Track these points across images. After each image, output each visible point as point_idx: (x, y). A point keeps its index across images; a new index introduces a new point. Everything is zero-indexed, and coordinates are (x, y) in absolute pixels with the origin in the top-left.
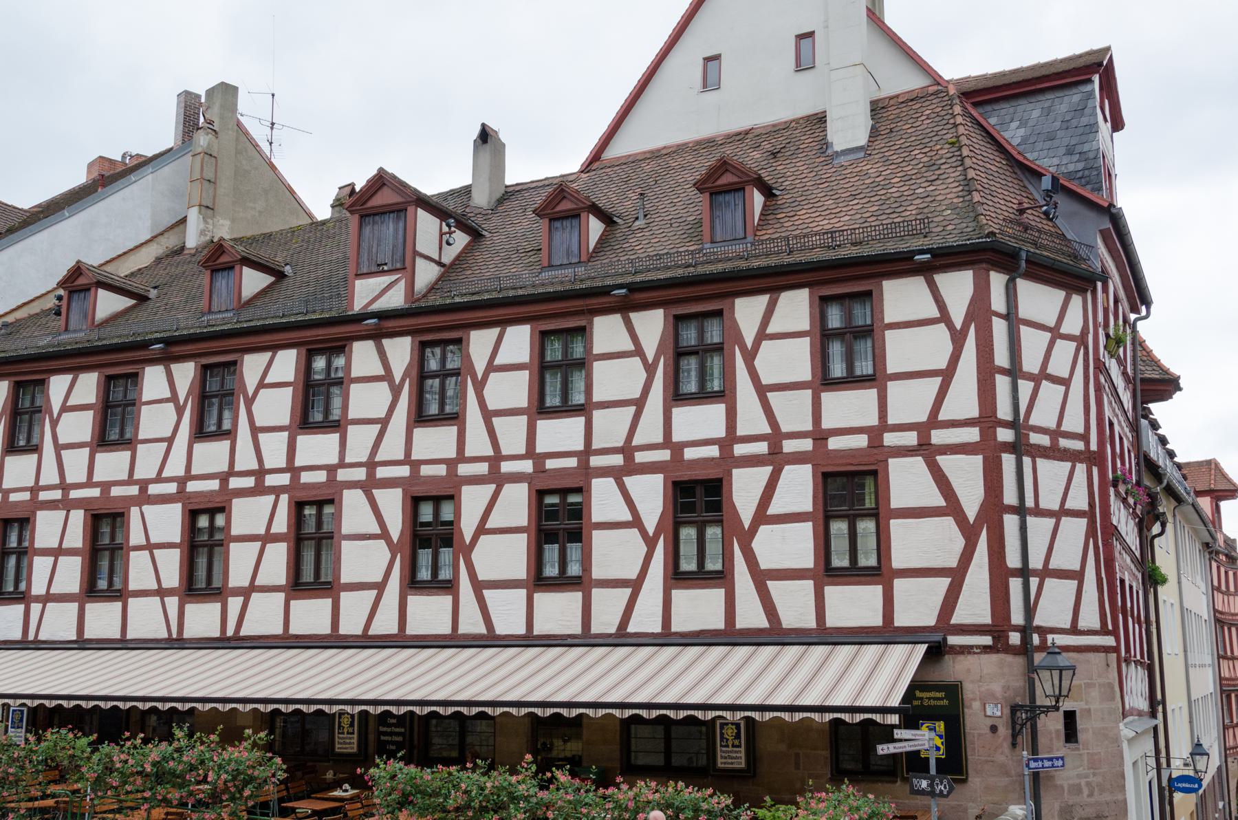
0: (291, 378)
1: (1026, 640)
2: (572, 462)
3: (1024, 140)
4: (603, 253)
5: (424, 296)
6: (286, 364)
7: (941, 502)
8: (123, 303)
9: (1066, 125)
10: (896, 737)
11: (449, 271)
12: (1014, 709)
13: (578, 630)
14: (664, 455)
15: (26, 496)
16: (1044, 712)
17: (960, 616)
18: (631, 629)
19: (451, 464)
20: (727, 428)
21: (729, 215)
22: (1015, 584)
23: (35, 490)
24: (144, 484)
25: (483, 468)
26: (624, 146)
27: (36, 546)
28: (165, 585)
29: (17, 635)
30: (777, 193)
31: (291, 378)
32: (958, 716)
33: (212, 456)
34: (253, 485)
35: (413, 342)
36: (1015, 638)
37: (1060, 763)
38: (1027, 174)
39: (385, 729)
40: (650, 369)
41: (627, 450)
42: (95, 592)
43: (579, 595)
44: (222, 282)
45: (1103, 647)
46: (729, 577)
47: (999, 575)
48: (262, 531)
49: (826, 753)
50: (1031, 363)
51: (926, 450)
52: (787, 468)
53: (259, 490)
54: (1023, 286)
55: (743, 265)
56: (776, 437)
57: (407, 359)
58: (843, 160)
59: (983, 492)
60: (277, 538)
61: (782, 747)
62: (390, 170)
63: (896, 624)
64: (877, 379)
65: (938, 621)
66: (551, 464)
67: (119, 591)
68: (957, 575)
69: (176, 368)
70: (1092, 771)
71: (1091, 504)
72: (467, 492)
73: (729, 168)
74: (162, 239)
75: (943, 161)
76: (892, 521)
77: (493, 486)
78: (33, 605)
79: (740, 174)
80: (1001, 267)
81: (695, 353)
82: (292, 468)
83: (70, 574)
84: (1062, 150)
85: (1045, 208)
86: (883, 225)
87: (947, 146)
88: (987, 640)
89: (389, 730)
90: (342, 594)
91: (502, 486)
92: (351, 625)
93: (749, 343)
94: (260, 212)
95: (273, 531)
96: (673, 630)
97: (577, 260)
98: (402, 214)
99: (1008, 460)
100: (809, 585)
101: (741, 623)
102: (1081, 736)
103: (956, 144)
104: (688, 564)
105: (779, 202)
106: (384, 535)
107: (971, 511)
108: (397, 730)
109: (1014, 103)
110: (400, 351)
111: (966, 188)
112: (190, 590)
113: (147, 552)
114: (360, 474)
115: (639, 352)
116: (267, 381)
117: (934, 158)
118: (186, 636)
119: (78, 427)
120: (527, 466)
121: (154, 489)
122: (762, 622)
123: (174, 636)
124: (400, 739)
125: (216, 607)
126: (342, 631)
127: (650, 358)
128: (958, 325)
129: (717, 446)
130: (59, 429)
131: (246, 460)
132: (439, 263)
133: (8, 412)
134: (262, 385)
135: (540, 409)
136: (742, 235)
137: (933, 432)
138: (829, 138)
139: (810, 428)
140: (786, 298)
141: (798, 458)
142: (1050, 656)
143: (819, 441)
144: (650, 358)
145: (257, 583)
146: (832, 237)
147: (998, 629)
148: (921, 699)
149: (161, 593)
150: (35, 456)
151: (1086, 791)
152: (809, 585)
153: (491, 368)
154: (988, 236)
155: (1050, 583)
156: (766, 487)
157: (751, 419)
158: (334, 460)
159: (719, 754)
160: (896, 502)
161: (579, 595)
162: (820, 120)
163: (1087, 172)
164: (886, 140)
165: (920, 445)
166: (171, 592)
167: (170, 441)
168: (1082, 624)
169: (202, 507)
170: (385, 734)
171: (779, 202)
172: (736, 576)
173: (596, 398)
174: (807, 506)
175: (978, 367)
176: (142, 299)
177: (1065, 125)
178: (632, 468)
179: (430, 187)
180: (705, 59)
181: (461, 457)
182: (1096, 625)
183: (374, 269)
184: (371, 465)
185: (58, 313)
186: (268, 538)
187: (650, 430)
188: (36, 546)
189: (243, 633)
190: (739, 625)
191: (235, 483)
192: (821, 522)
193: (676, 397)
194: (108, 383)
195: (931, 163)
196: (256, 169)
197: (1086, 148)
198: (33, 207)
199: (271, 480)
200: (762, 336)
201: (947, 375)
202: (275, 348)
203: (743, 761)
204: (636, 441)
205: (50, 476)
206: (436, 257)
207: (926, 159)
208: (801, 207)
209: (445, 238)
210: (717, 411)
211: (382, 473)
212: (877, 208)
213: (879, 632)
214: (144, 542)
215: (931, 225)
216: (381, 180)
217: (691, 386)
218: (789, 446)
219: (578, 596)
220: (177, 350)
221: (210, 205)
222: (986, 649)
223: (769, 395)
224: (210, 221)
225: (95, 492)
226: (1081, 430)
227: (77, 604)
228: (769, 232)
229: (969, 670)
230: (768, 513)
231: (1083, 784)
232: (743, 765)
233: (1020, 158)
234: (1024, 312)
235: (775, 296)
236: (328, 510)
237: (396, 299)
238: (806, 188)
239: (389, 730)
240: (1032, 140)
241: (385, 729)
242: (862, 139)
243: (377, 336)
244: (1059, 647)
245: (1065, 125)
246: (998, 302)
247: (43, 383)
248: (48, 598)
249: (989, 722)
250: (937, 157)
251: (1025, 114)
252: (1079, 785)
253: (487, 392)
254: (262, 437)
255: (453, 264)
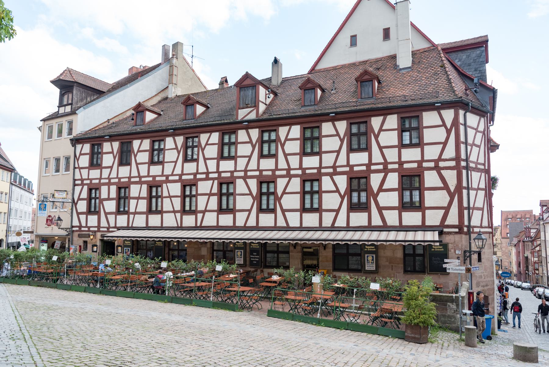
0: (217, 142)
1: (469, 230)
2: (315, 171)
3: (461, 65)
4: (322, 102)
5: (262, 115)
6: (215, 137)
7: (442, 185)
8: (154, 116)
9: (475, 61)
10: (445, 261)
11: (269, 106)
12: (465, 252)
13: (318, 225)
14: (347, 169)
15: (127, 180)
16: (475, 253)
17: (448, 222)
18: (336, 225)
19: (273, 171)
20: (369, 160)
21: (367, 89)
22: (466, 212)
23: (130, 178)
24: (167, 176)
25: (284, 173)
26: (326, 64)
27: (131, 196)
28: (176, 209)
29: (126, 225)
30: (381, 82)
31: (217, 142)
32: (447, 254)
33: (190, 167)
34: (205, 177)
35: (259, 130)
36: (465, 229)
37: (478, 269)
38: (465, 78)
39: (253, 256)
40: (342, 141)
41: (334, 167)
42: (151, 211)
43: (318, 214)
44: (189, 109)
45: (489, 232)
46: (369, 209)
47: (461, 209)
48: (209, 192)
49: (402, 265)
50: (470, 141)
51: (437, 168)
52: (389, 174)
53: (207, 179)
54: (468, 114)
55: (374, 106)
56: (386, 163)
57: (257, 136)
58: (403, 71)
59: (456, 182)
60: (214, 195)
61: (387, 263)
62: (249, 72)
63: (426, 225)
64: (420, 144)
65: (440, 224)
66: (308, 171)
67: (160, 211)
68: (447, 209)
69: (177, 138)
70: (485, 271)
71: (486, 187)
72: (279, 180)
73: (367, 73)
74: (160, 95)
75: (440, 72)
76: (425, 191)
77: (288, 179)
78: (130, 215)
79: (371, 76)
80: (463, 109)
81: (409, 131)
82: (218, 172)
83: (143, 206)
84: (474, 70)
85: (475, 89)
86: (417, 94)
87: (439, 67)
88: (457, 230)
89: (254, 257)
90: (237, 213)
91: (291, 178)
92: (240, 222)
93: (376, 132)
94: (190, 86)
95: (212, 192)
96: (350, 226)
97: (314, 104)
98: (254, 87)
99: (464, 172)
100: (397, 212)
101: (278, 225)
102: (482, 260)
103: (443, 66)
104: (264, 206)
105: (383, 85)
106: (251, 194)
107: (452, 189)
108: (257, 257)
109: (457, 53)
110: (255, 133)
111: (449, 82)
112: (119, 211)
113: (169, 199)
114: (242, 174)
115: (338, 134)
116: (209, 143)
117: (436, 71)
118: (164, 226)
119: (144, 157)
120: (299, 172)
121: (171, 178)
122: (381, 223)
123: (179, 226)
124: (258, 260)
125: (193, 217)
126: (237, 225)
127: (342, 137)
128: (449, 127)
129: (365, 166)
130: (137, 158)
131: (202, 169)
132: (266, 104)
133: (119, 152)
134: (207, 144)
135: (303, 153)
136: (372, 96)
137: (440, 163)
138: (398, 64)
139: (398, 161)
140: (294, 127)
141: (393, 171)
142: (479, 235)
143: (401, 165)
144: (342, 137)
145: (207, 209)
146: (405, 97)
147: (460, 227)
148: (367, 248)
149: (174, 212)
150: (129, 167)
151: (483, 277)
152: (397, 212)
153: (287, 139)
154: (459, 98)
155: (475, 211)
156: (382, 180)
157: (377, 157)
158: (233, 169)
159: (366, 265)
160: (427, 185)
161: (318, 214)
162: (394, 57)
163: (481, 77)
164: (418, 65)
165: (435, 167)
166: (178, 212)
167: (176, 162)
168: (483, 225)
169: (188, 184)
170: (253, 258)
171: (383, 85)
172: (372, 208)
173: (323, 150)
174: (396, 186)
175: (455, 141)
176: (159, 115)
177: (474, 61)
178: (336, 173)
179: (259, 77)
180: (351, 36)
181: (277, 169)
182: (487, 225)
183: (245, 106)
184: (246, 171)
185: (133, 119)
186: (210, 194)
187: (342, 160)
188: (131, 196)
189: (203, 225)
190: (373, 224)
191: (199, 176)
192: (219, 196)
193: (351, 150)
194: (122, 144)
195: (435, 73)
196: (188, 71)
197: (481, 69)
198: (114, 83)
199: (211, 176)
200: (381, 130)
201: (445, 144)
202: (211, 132)
203: (374, 268)
204: (337, 165)
205: (134, 173)
206: (265, 102)
207: (433, 72)
208: (391, 87)
209: (267, 96)
210: (365, 155)
211: (249, 174)
212: (418, 88)
213: (420, 227)
214: (168, 195)
215: (439, 94)
216: (247, 76)
217: (355, 146)
218: (390, 167)
219: (160, 216)
220: (177, 132)
221: (176, 83)
222: (456, 233)
223: (383, 150)
224: (176, 89)
225: (151, 179)
226: (483, 162)
227: (145, 215)
228: (381, 95)
229: (450, 239)
230: (383, 188)
231: (483, 275)
232: (374, 269)
233: (463, 72)
234: (468, 123)
235: (385, 117)
236: (363, 181)
237: (253, 116)
238: (391, 81)
239: (254, 257)
240: (463, 66)
241: (253, 256)
242: (409, 64)
243: (247, 128)
244: (482, 232)
245: (474, 61)
246: (461, 120)
247: (131, 143)
248: (135, 213)
249: (457, 256)
250: (437, 71)
251: (461, 57)
252: (481, 275)
253: (285, 147)
254: (207, 161)
255: (269, 104)
